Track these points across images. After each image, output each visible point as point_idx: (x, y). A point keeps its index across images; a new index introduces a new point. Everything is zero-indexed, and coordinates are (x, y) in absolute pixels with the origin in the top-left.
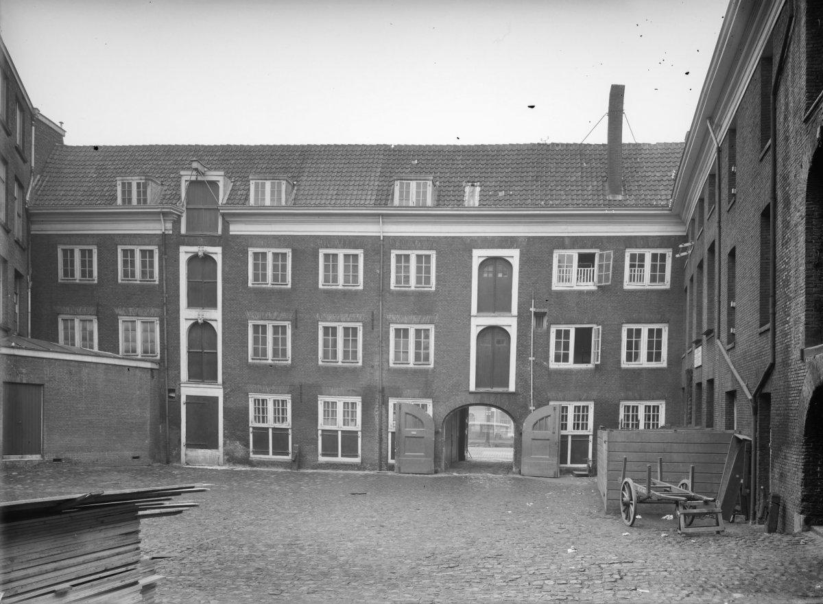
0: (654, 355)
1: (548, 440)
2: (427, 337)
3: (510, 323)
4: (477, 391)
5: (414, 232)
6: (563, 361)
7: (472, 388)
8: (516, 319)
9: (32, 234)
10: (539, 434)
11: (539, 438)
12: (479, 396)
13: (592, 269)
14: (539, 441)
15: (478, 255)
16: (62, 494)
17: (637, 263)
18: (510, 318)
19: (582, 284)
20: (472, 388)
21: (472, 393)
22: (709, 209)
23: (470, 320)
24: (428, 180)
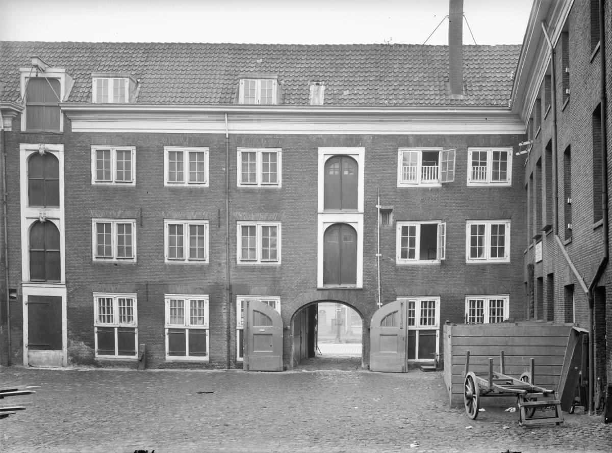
0: (497, 251)
1: (396, 335)
4: (324, 288)
7: (320, 284)
10: (387, 329)
12: (327, 292)
19: (427, 181)
21: (319, 290)
24: (273, 79)
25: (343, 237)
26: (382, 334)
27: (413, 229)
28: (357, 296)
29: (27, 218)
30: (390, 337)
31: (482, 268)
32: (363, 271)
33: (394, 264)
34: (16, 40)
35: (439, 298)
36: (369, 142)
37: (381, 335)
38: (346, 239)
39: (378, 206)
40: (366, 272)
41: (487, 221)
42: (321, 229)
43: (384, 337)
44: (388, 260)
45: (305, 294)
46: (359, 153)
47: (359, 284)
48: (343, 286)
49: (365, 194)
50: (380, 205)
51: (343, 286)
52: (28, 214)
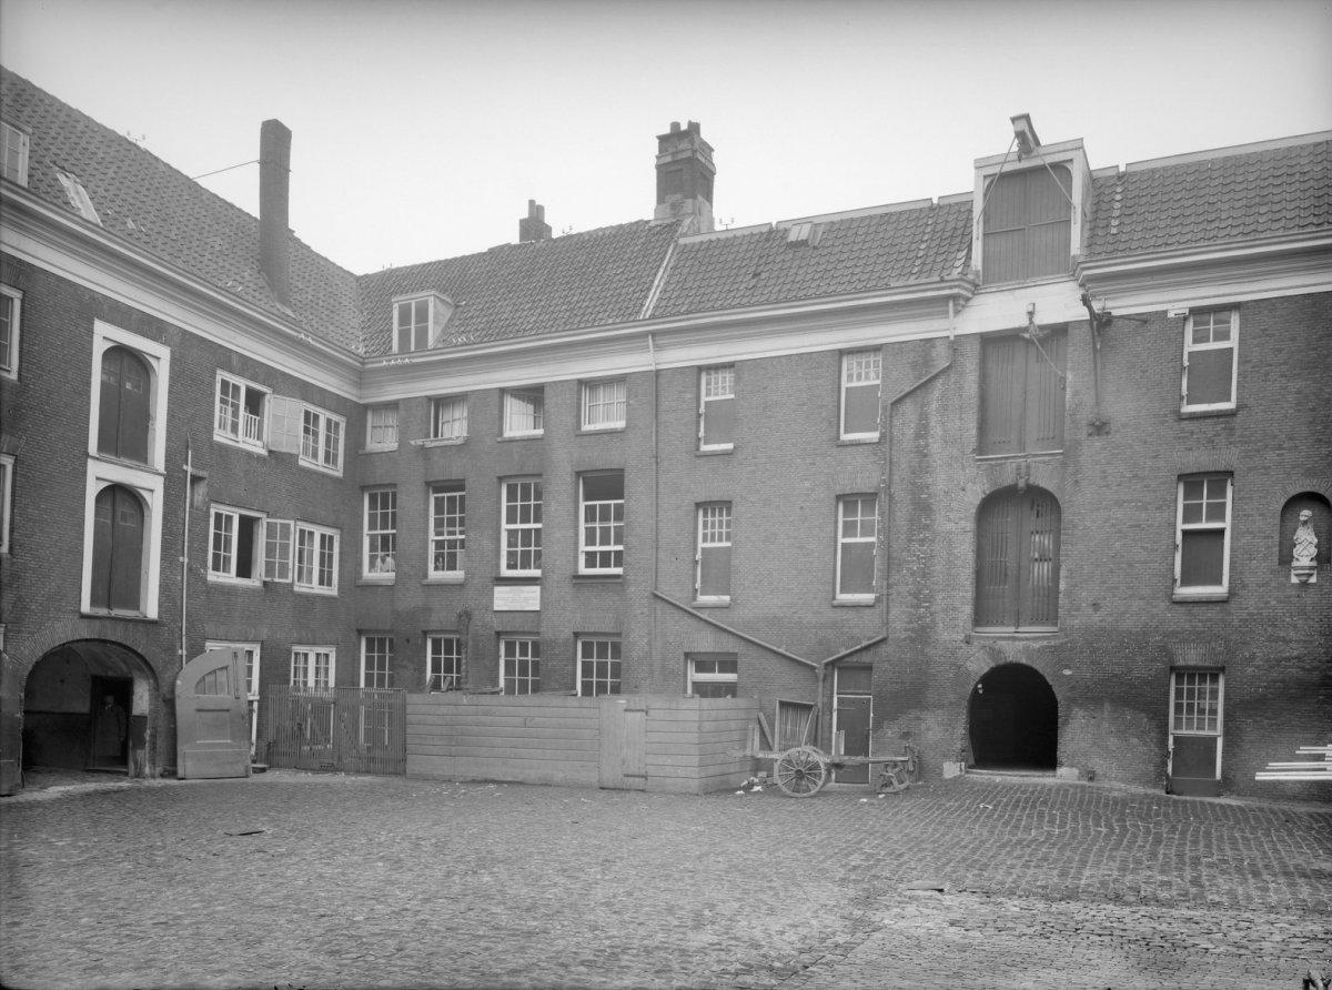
0: (325, 579)
1: (228, 710)
2: (511, 555)
3: (151, 485)
4: (92, 613)
5: (97, 284)
6: (224, 571)
7: (86, 607)
8: (161, 479)
9: (1258, 781)
10: (210, 699)
11: (212, 707)
12: (97, 623)
13: (258, 418)
14: (210, 714)
15: (104, 334)
16: (744, 632)
17: (612, 524)
18: (152, 476)
19: (251, 440)
20: (86, 607)
21: (84, 617)
22: (1319, 814)
23: (85, 465)
24: (23, 131)
25: (119, 514)
26: (200, 708)
27: (229, 518)
28: (148, 635)
29: (98, 479)
30: (216, 713)
31: (310, 600)
32: (160, 586)
33: (204, 580)
34: (30, 80)
35: (259, 645)
36: (177, 339)
37: (199, 710)
38: (124, 517)
39: (189, 469)
40: (165, 588)
41: (318, 527)
42: (92, 490)
43: (202, 714)
44: (196, 575)
45: (58, 625)
46: (160, 356)
47: (151, 610)
48: (117, 612)
49: (168, 439)
50: (192, 466)
51: (117, 612)
52: (101, 472)
